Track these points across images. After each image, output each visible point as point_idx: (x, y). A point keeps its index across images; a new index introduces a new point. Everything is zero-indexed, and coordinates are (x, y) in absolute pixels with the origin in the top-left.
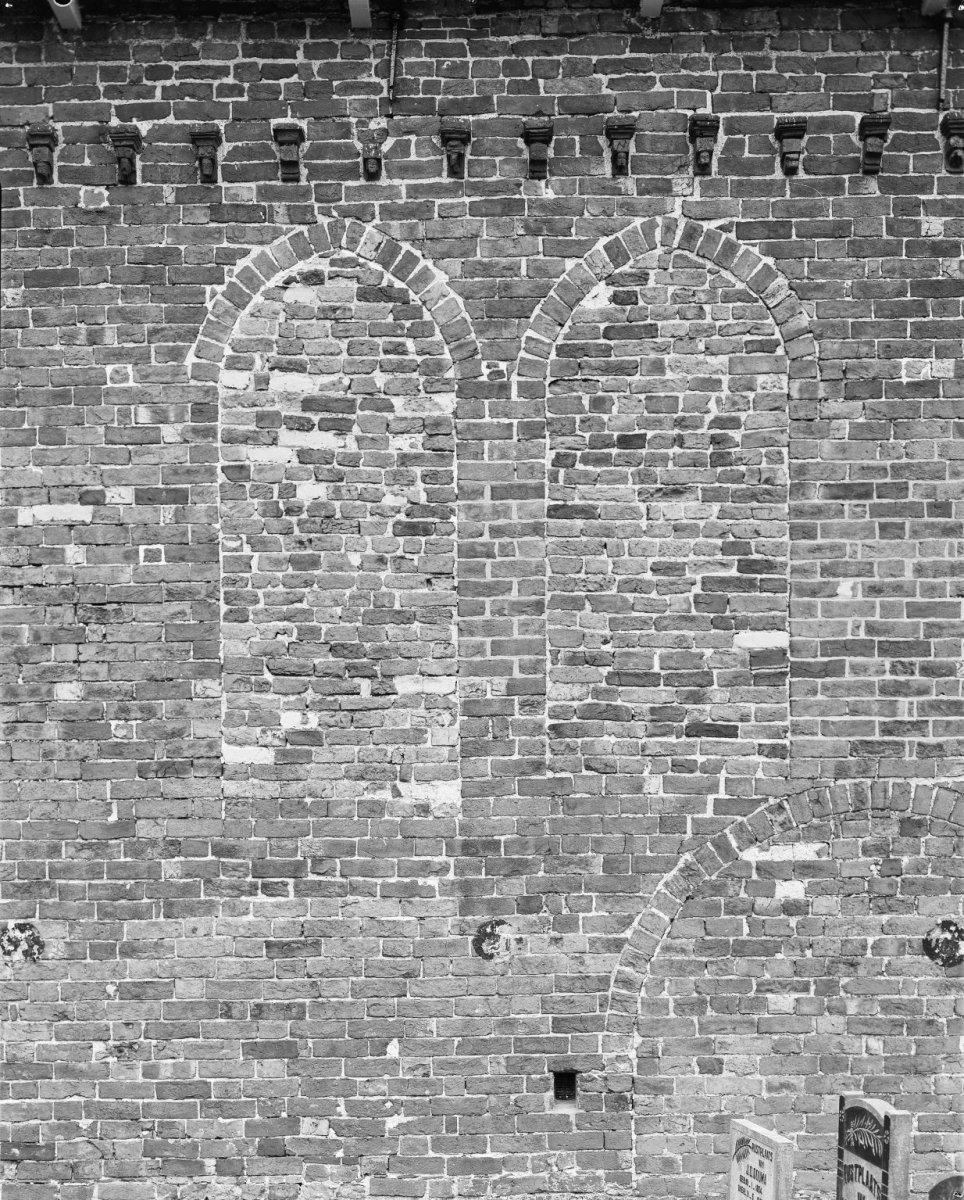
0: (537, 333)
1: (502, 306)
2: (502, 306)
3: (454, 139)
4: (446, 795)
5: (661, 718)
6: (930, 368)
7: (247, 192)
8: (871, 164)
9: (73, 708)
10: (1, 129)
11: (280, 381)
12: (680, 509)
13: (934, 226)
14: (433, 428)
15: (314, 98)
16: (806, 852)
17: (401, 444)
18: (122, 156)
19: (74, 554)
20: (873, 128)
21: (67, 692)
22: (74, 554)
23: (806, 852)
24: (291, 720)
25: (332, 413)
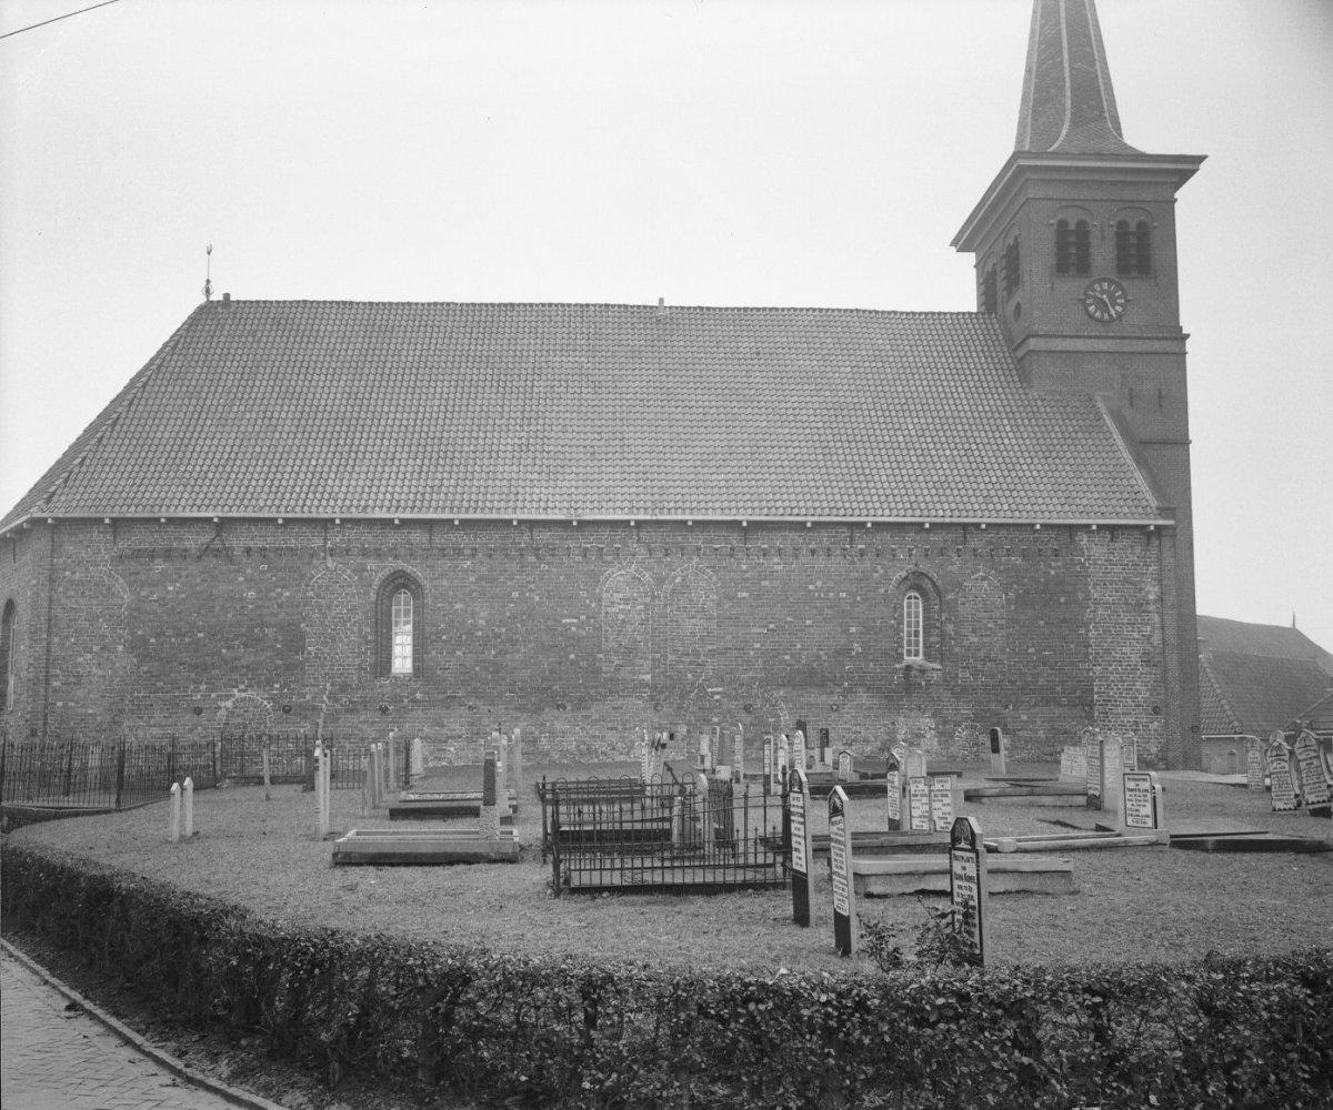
0: (667, 587)
1: (660, 581)
2: (660, 581)
3: (650, 551)
4: (649, 677)
5: (691, 663)
6: (744, 594)
7: (609, 558)
8: (732, 556)
9: (570, 851)
10: (1331, 719)
11: (616, 595)
12: (694, 621)
13: (744, 567)
14: (645, 604)
15: (623, 541)
16: (720, 689)
17: (639, 607)
18: (585, 553)
19: (574, 629)
20: (732, 549)
21: (572, 656)
22: (574, 629)
23: (720, 689)
24: (617, 662)
25: (626, 601)
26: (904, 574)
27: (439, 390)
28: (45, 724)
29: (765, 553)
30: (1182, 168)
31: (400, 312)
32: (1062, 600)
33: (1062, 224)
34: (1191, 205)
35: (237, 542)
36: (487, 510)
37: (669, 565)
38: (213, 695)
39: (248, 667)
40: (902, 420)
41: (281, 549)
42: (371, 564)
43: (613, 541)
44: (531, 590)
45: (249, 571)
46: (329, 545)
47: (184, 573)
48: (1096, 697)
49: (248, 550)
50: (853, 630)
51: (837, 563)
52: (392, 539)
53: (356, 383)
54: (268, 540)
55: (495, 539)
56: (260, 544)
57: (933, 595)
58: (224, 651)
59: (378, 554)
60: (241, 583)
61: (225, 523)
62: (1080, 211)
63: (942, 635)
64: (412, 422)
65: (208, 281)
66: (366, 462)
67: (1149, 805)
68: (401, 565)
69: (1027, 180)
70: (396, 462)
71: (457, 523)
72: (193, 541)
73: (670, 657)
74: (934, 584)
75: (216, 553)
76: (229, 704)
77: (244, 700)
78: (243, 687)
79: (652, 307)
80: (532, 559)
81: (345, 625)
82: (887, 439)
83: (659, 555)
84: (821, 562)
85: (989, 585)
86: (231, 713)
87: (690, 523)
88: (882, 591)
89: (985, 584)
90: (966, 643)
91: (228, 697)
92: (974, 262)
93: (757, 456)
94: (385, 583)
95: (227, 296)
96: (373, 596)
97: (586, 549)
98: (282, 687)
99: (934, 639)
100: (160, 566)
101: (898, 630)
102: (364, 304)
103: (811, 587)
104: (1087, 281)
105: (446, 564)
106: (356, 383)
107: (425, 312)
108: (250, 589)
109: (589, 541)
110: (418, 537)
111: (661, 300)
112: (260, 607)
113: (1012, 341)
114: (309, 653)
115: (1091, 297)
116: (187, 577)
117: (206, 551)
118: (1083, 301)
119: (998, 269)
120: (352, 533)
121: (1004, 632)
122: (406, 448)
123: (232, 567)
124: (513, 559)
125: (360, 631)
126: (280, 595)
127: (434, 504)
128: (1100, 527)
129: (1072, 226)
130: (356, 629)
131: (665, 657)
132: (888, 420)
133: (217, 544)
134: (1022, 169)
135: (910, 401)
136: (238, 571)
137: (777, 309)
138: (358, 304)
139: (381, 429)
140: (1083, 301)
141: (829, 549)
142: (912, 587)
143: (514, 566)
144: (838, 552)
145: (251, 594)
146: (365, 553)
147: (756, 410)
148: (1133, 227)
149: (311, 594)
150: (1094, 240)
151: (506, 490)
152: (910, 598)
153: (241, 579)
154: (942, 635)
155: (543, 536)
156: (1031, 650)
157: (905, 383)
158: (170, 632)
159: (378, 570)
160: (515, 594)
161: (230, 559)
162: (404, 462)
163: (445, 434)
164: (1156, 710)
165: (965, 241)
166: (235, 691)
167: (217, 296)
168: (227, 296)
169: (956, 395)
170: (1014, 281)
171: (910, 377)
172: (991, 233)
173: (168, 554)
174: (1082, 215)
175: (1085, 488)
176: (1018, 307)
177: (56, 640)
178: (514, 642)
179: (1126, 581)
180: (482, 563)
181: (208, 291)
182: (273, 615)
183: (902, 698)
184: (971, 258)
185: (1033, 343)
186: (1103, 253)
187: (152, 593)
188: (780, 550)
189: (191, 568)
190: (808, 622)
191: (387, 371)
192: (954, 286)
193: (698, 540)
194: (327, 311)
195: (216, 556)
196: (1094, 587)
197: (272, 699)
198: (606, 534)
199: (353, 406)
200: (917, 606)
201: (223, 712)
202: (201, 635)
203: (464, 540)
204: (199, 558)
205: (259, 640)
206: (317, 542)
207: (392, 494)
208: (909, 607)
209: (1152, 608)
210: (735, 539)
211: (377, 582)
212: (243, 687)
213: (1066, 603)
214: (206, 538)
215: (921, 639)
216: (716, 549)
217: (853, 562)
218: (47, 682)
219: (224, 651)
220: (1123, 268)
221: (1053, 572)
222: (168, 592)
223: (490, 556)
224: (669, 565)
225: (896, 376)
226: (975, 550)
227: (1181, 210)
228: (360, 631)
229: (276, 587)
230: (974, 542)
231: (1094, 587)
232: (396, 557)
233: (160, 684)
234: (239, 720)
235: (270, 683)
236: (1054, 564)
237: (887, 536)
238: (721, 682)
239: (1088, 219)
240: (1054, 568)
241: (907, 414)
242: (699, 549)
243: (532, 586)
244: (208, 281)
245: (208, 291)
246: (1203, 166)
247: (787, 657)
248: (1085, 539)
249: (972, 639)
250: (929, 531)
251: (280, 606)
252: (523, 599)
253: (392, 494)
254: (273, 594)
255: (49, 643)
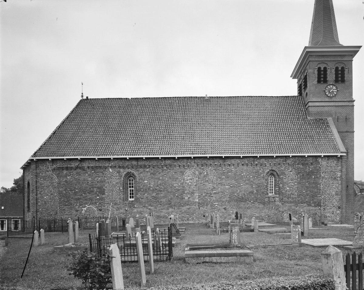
0: (202, 175)
1: (200, 174)
2: (200, 174)
3: (198, 165)
5: (209, 196)
6: (224, 177)
7: (186, 168)
12: (210, 184)
13: (224, 169)
14: (196, 180)
15: (190, 163)
16: (217, 203)
18: (180, 166)
19: (177, 187)
21: (176, 195)
22: (177, 187)
23: (217, 203)
24: (189, 196)
26: (268, 170)
27: (143, 122)
28: (37, 215)
29: (229, 165)
30: (354, 51)
31: (134, 100)
32: (313, 177)
33: (319, 69)
34: (357, 62)
35: (85, 165)
36: (174, 154)
37: (203, 169)
38: (81, 206)
39: (90, 199)
40: (271, 127)
41: (97, 167)
42: (122, 170)
43: (187, 163)
44: (165, 177)
45: (89, 173)
46: (110, 165)
47: (72, 174)
48: (322, 204)
49: (88, 167)
50: (254, 186)
51: (250, 168)
52: (127, 163)
53: (121, 121)
54: (92, 164)
55: (155, 163)
56: (92, 165)
57: (277, 176)
58: (83, 195)
59: (123, 168)
60: (87, 176)
61: (82, 160)
62: (324, 64)
63: (279, 187)
64: (135, 131)
65: (82, 94)
66: (121, 142)
67: (298, 235)
68: (130, 170)
69: (310, 55)
70: (129, 142)
71: (144, 158)
72: (74, 165)
73: (203, 195)
74: (277, 173)
75: (80, 168)
76: (85, 209)
77: (89, 208)
78: (88, 204)
79: (204, 97)
80: (165, 168)
81: (115, 187)
82: (266, 132)
83: (200, 166)
84: (245, 167)
85: (293, 173)
86: (86, 211)
87: (208, 157)
88: (262, 175)
89: (291, 173)
90: (286, 190)
91: (85, 207)
92: (297, 82)
93: (229, 138)
94: (126, 175)
95: (87, 97)
96: (122, 179)
97: (180, 165)
98: (99, 204)
99: (276, 189)
100: (65, 172)
101: (267, 186)
102: (125, 99)
103: (242, 175)
104: (326, 85)
105: (141, 170)
106: (121, 121)
107: (141, 100)
108: (90, 177)
109: (181, 163)
110: (134, 163)
111: (206, 95)
112: (93, 182)
113: (305, 103)
114: (106, 195)
115: (327, 90)
116: (73, 174)
117: (77, 167)
118: (325, 91)
119: (302, 82)
120: (116, 162)
121: (297, 186)
122: (132, 138)
123: (84, 172)
124: (160, 168)
125: (119, 189)
126: (98, 179)
127: (138, 153)
128: (324, 156)
129: (322, 69)
130: (118, 188)
131: (202, 195)
132: (267, 127)
133: (80, 166)
134: (308, 52)
135: (274, 122)
136: (86, 173)
137: (239, 97)
138: (123, 99)
139: (126, 133)
140: (325, 91)
141: (247, 164)
142: (271, 174)
143: (160, 170)
144: (250, 165)
145: (90, 179)
146: (120, 167)
147: (230, 125)
148: (322, 69)
149: (106, 179)
150: (328, 72)
151: (158, 149)
152: (270, 177)
153: (87, 175)
154: (279, 187)
155: (168, 162)
156: (304, 191)
157: (273, 117)
158: (69, 190)
159: (124, 172)
160: (161, 178)
161: (84, 170)
162: (131, 142)
163: (143, 134)
164: (339, 208)
165: (294, 76)
166: (87, 205)
167: (85, 98)
168: (87, 97)
169: (287, 120)
170: (306, 86)
171: (275, 115)
172: (301, 73)
173: (67, 168)
174: (325, 66)
175: (321, 145)
176: (307, 93)
177: (39, 192)
178: (161, 191)
179: (331, 171)
180: (152, 170)
181: (82, 96)
182: (96, 184)
183: (268, 205)
184: (296, 80)
185: (310, 104)
186: (331, 76)
187: (63, 179)
188: (234, 164)
189: (74, 172)
190: (242, 184)
191: (129, 117)
192: (291, 88)
193: (210, 162)
194: (114, 101)
195: (80, 169)
196: (322, 173)
197: (96, 207)
198: (185, 160)
199: (167, 129)
200: (272, 179)
201: (84, 211)
202: (77, 190)
203: (147, 163)
204: (76, 169)
205: (93, 191)
206: (107, 165)
207: (127, 151)
208: (270, 179)
209: (339, 179)
210: (221, 161)
211: (124, 175)
212: (88, 204)
213: (314, 178)
214: (77, 164)
215: (273, 189)
216: (216, 164)
217: (254, 167)
218: (37, 204)
219: (83, 195)
220: (337, 81)
221: (311, 169)
222: (68, 179)
223: (154, 168)
224: (203, 169)
225: (271, 115)
226: (289, 163)
227: (354, 63)
228: (119, 189)
229: (96, 177)
230: (288, 161)
231: (322, 173)
232: (128, 168)
233: (67, 204)
234: (88, 213)
235: (96, 203)
236: (311, 167)
237: (263, 160)
238: (218, 201)
239: (344, 66)
240: (311, 168)
241: (273, 125)
242: (211, 164)
243: (165, 176)
244: (82, 94)
245: (82, 96)
246: (361, 50)
247: (235, 194)
248: (320, 160)
249: (288, 188)
250: (242, 158)
251: (98, 182)
252: (163, 180)
253: (127, 151)
254: (96, 179)
255: (37, 193)
